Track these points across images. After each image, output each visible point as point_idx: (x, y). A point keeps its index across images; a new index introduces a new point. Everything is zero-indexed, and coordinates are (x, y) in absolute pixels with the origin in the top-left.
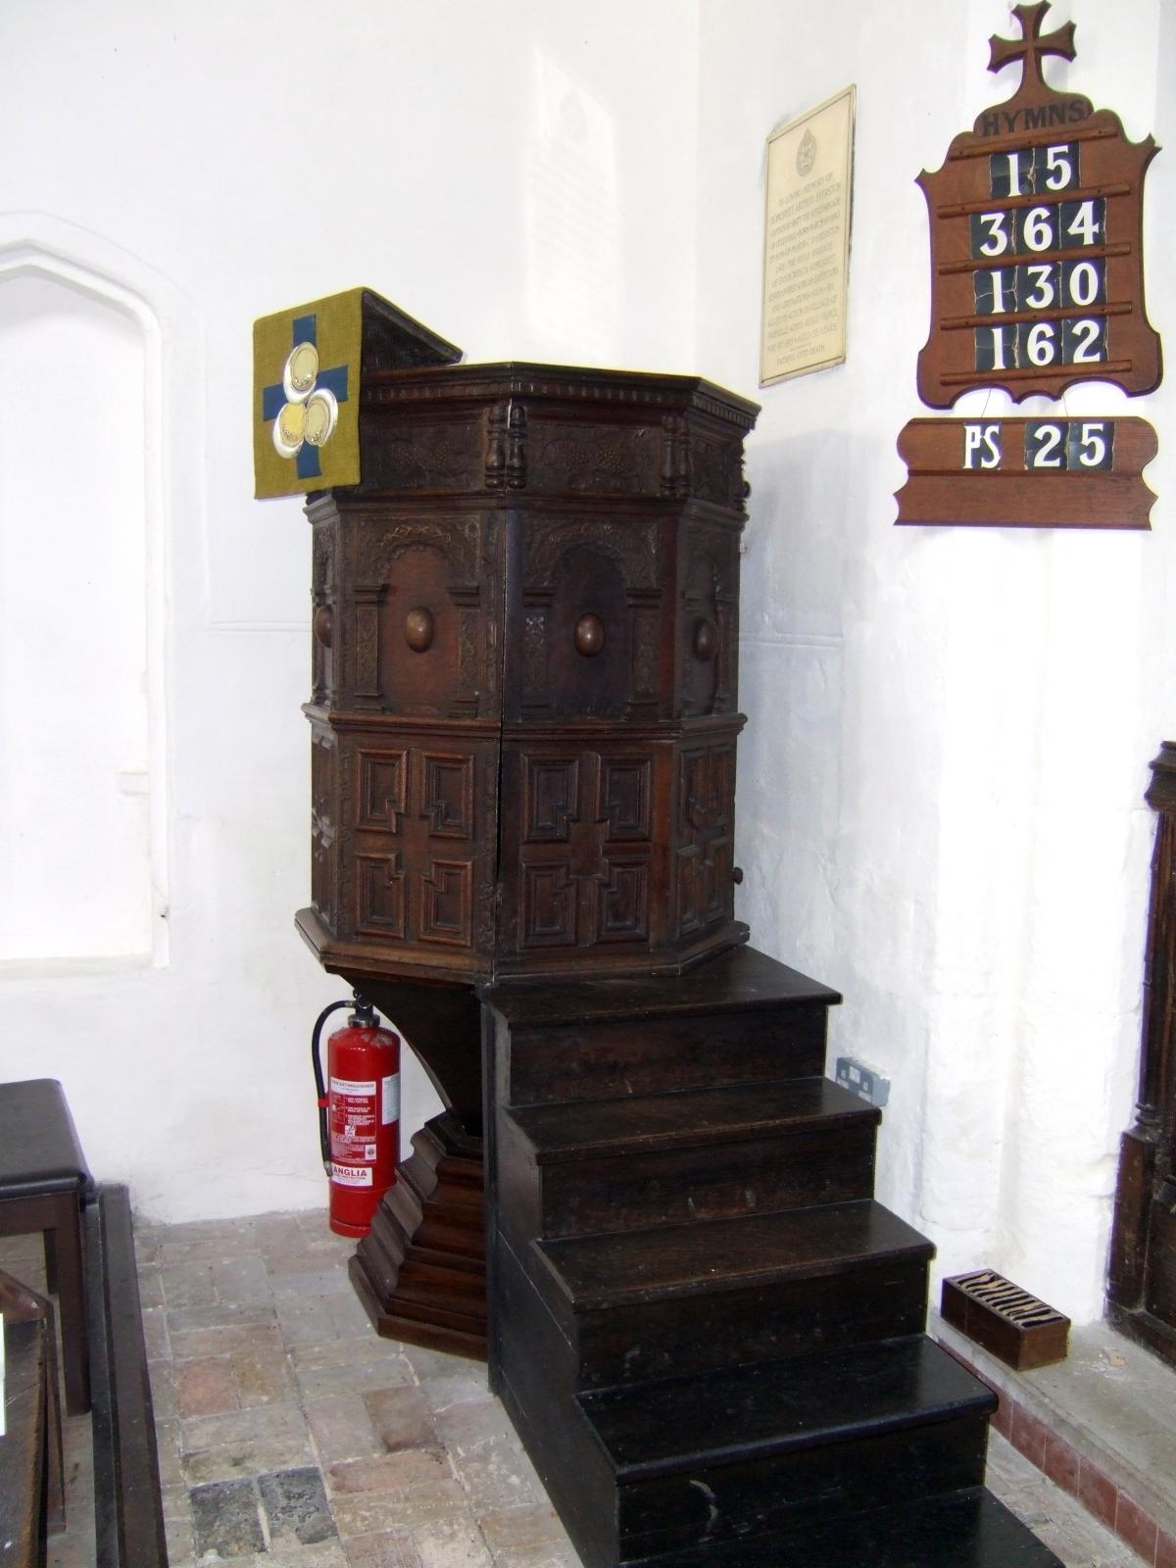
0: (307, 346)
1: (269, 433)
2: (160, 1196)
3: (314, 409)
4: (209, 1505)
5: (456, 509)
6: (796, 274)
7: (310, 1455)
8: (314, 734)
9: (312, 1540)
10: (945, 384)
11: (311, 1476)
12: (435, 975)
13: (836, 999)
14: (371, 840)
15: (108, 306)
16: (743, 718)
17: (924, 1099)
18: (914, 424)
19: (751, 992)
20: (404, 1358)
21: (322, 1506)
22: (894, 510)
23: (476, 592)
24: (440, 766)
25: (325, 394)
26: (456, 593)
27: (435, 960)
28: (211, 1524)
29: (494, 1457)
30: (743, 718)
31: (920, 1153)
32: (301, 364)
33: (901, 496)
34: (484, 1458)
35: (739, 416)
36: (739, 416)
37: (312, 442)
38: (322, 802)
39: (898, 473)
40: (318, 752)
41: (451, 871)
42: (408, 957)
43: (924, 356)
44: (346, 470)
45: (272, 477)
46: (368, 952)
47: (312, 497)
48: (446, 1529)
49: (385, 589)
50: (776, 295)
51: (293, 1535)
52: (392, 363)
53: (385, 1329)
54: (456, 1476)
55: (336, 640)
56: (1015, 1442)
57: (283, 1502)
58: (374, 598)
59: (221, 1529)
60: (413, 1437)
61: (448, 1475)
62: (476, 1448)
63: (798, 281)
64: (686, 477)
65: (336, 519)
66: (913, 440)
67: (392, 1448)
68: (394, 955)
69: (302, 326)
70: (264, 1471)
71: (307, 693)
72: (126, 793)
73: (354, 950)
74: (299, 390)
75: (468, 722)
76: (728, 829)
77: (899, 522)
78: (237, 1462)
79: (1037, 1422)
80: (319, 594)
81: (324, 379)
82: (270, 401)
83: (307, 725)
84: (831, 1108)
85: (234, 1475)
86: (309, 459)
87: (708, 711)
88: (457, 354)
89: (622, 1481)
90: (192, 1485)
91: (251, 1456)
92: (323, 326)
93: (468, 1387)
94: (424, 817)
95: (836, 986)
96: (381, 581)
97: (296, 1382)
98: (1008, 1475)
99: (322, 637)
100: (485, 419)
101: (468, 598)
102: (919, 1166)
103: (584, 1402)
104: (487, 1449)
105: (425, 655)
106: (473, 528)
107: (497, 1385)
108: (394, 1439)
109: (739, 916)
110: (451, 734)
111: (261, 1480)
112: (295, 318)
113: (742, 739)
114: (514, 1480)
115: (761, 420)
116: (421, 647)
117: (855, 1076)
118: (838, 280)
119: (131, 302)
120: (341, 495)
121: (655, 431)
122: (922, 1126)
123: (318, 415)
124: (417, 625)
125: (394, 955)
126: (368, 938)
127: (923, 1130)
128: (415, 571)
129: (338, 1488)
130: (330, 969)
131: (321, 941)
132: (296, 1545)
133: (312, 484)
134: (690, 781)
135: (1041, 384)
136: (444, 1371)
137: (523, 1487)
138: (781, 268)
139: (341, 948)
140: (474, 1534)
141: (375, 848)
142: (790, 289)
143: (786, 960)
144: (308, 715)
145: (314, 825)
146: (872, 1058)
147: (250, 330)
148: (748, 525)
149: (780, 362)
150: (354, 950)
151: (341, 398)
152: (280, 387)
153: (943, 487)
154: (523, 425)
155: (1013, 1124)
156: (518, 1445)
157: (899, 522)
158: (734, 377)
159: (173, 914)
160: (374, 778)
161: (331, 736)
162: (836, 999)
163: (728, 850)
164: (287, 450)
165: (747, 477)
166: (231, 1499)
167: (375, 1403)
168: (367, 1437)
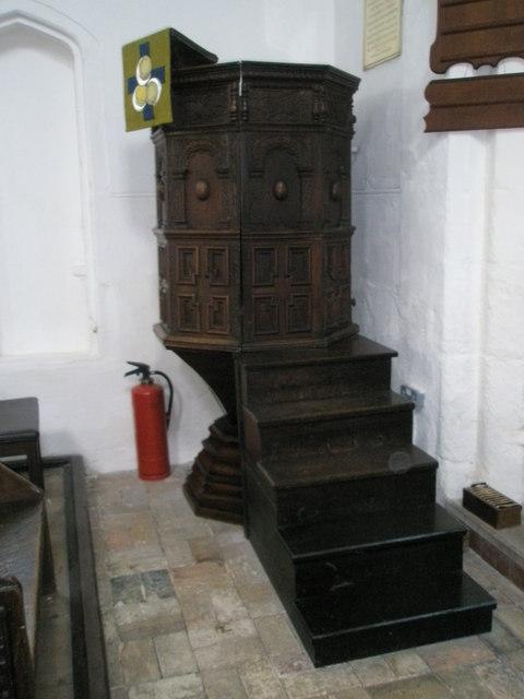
0: (146, 57)
1: (131, 98)
2: (128, 374)
3: (151, 88)
4: (119, 584)
5: (217, 133)
6: (379, 12)
7: (164, 564)
8: (159, 242)
9: (164, 597)
10: (443, 61)
11: (164, 572)
12: (215, 348)
13: (396, 355)
14: (184, 288)
15: (52, 43)
16: (354, 228)
17: (440, 402)
18: (433, 83)
19: (358, 351)
20: (207, 527)
21: (169, 584)
22: (423, 125)
23: (225, 172)
24: (215, 253)
25: (155, 80)
26: (218, 172)
27: (214, 342)
28: (119, 592)
29: (245, 564)
30: (354, 228)
31: (439, 426)
32: (144, 65)
33: (427, 118)
34: (241, 564)
35: (348, 84)
36: (348, 84)
37: (150, 103)
38: (162, 275)
39: (424, 107)
40: (161, 251)
41: (220, 302)
42: (203, 341)
43: (434, 49)
44: (166, 116)
45: (133, 121)
46: (185, 339)
47: (154, 129)
48: (223, 593)
49: (187, 172)
50: (371, 24)
51: (156, 596)
52: (185, 64)
53: (198, 513)
54: (229, 571)
55: (166, 197)
56: (484, 556)
57: (152, 582)
58: (181, 176)
59: (124, 594)
60: (210, 557)
61: (225, 572)
62: (239, 560)
63: (378, 16)
64: (325, 113)
65: (164, 141)
66: (433, 92)
67: (200, 561)
68: (196, 340)
69: (144, 47)
70: (143, 571)
71: (154, 223)
72: (76, 275)
73: (178, 339)
74: (144, 79)
75: (226, 232)
76: (348, 280)
77: (426, 131)
78: (132, 567)
79: (493, 546)
80: (159, 177)
81: (154, 73)
82: (131, 84)
83: (155, 238)
84: (395, 402)
85: (129, 573)
86: (149, 112)
87: (338, 225)
88: (216, 58)
89: (296, 562)
90: (112, 577)
91: (137, 565)
92: (152, 47)
93: (236, 536)
94: (207, 277)
95: (395, 349)
96: (184, 168)
97: (159, 536)
98: (474, 567)
99: (161, 196)
100: (229, 90)
101: (223, 174)
102: (439, 433)
103: (280, 531)
104: (243, 561)
105: (205, 203)
106: (225, 142)
107: (248, 535)
108: (201, 558)
109: (355, 320)
110: (217, 237)
111: (142, 574)
112: (306, 661)
113: (354, 238)
114: (255, 573)
115: (361, 86)
116: (203, 198)
117: (409, 393)
118: (397, 14)
119: (67, 40)
120: (166, 128)
121: (309, 93)
122: (440, 415)
123: (153, 90)
124: (201, 187)
125: (196, 340)
126: (185, 333)
127: (440, 417)
128: (200, 162)
129: (176, 577)
130: (168, 348)
131: (163, 335)
132: (157, 599)
133: (152, 122)
134: (330, 259)
135: (489, 60)
136: (223, 530)
137: (257, 574)
138: (373, 9)
139: (172, 338)
140: (235, 594)
141: (185, 292)
142: (376, 21)
143: (378, 341)
144: (155, 234)
145: (160, 285)
146: (417, 385)
147: (120, 51)
148: (355, 136)
149: (372, 57)
150: (178, 339)
151: (162, 81)
152: (135, 78)
153: (453, 110)
154: (247, 91)
155: (481, 413)
156: (256, 559)
157: (426, 131)
158: (351, 67)
159: (99, 330)
160: (185, 260)
161: (165, 242)
162: (396, 355)
163: (348, 290)
164: (139, 108)
165: (354, 113)
166: (128, 582)
167: (193, 544)
168: (189, 557)
